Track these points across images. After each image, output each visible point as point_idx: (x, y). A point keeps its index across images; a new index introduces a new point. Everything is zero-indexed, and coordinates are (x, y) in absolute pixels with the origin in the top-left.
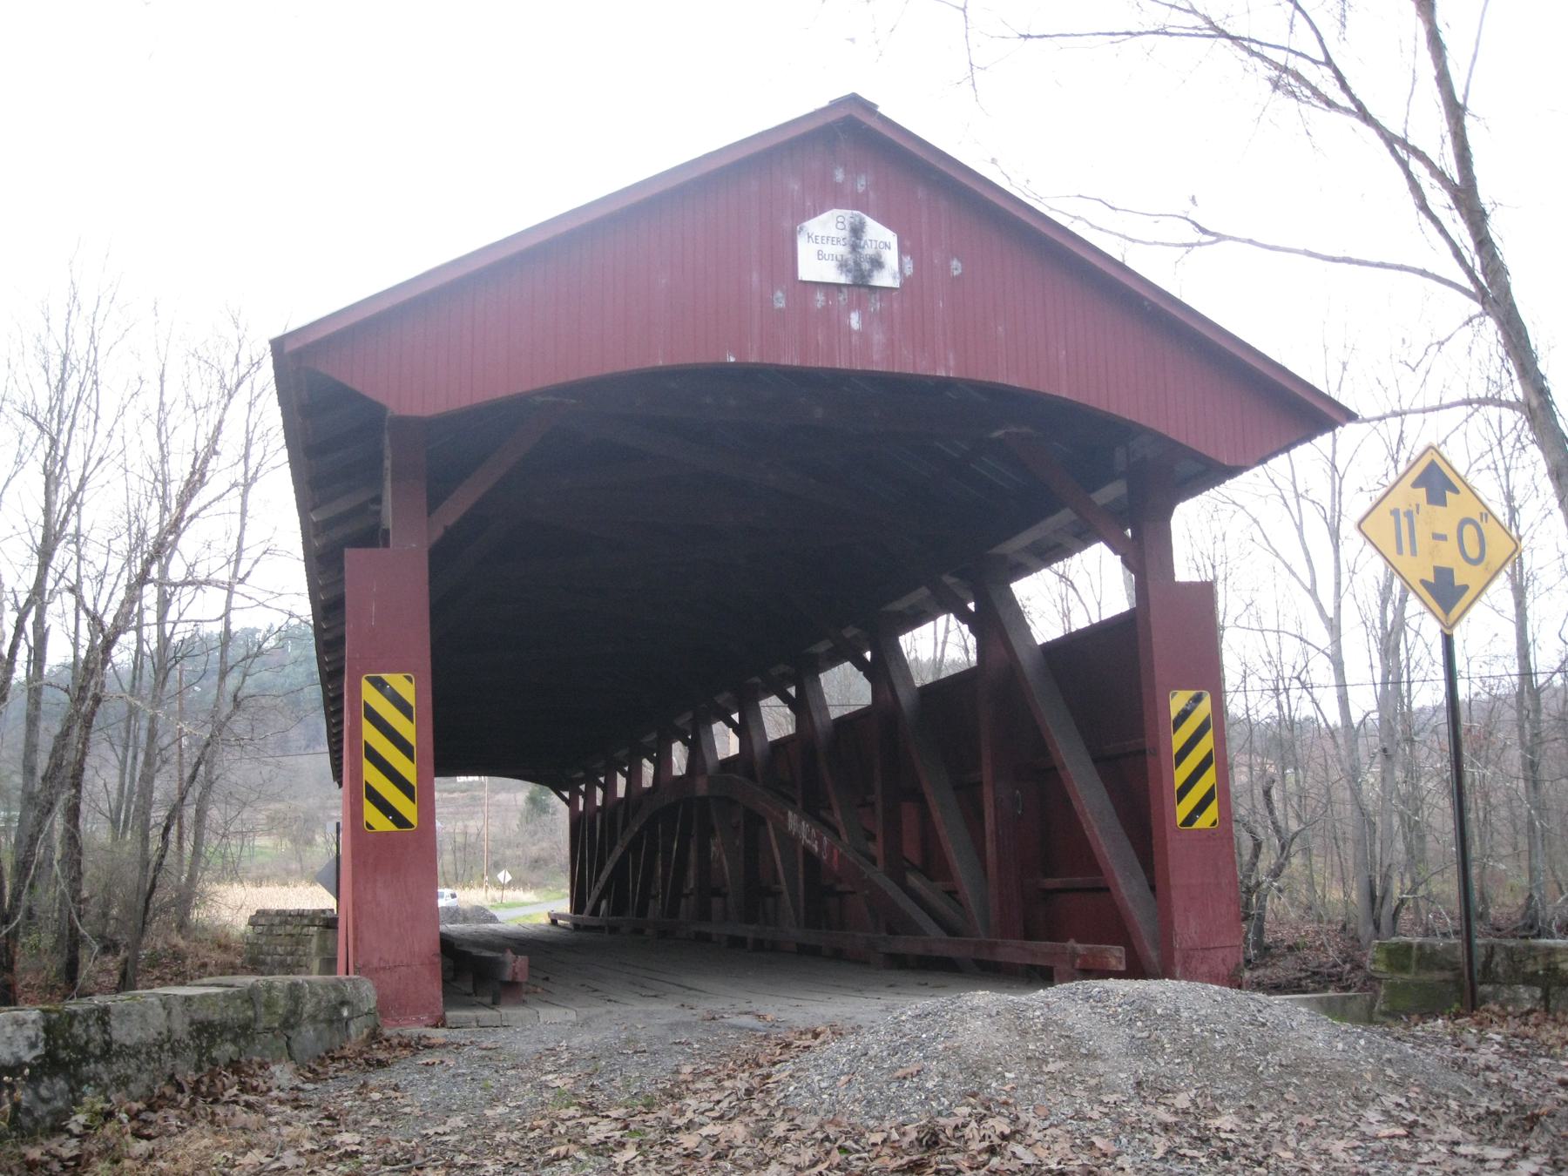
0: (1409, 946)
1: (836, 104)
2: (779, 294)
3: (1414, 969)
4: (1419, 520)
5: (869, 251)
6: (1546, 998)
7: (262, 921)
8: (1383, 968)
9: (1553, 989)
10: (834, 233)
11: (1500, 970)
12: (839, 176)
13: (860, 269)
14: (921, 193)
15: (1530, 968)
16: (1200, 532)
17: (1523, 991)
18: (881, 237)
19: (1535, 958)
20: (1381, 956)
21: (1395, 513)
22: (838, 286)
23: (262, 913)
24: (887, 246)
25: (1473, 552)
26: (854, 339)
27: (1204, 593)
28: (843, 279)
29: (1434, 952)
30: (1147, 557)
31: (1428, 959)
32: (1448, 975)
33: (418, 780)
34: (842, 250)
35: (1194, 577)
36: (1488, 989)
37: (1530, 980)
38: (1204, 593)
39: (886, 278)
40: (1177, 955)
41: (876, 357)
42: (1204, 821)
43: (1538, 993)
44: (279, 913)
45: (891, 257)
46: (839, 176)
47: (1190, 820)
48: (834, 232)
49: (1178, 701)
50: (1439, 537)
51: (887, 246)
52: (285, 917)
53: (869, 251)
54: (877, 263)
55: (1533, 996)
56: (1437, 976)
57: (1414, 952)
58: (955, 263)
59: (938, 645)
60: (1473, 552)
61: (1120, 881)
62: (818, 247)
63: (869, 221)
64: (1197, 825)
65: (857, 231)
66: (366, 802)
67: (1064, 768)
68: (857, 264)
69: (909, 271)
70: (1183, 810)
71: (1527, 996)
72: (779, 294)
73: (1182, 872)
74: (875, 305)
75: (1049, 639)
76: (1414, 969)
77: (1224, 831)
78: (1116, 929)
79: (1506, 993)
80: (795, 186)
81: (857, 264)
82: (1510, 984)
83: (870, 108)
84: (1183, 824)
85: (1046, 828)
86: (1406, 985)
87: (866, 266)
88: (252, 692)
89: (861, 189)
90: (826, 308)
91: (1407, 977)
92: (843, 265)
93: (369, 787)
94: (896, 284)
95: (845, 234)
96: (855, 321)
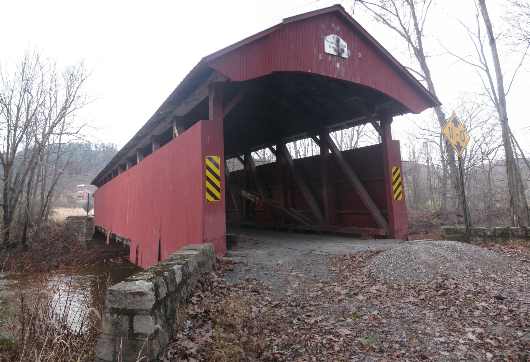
0: (451, 229)
1: (335, 6)
2: (320, 55)
4: (453, 130)
5: (341, 47)
6: (484, 240)
7: (70, 219)
10: (333, 41)
12: (333, 26)
13: (340, 52)
14: (351, 34)
15: (479, 234)
16: (402, 126)
18: (343, 43)
20: (444, 231)
21: (449, 128)
22: (334, 55)
23: (69, 217)
24: (345, 47)
25: (463, 139)
26: (338, 70)
27: (397, 142)
28: (335, 54)
29: (457, 230)
30: (384, 130)
32: (461, 235)
34: (335, 46)
35: (396, 139)
36: (471, 238)
37: (480, 236)
38: (397, 142)
39: (345, 55)
41: (343, 76)
42: (400, 199)
43: (482, 239)
44: (74, 217)
45: (346, 49)
46: (333, 26)
48: (333, 41)
50: (457, 135)
51: (345, 47)
52: (76, 218)
53: (341, 47)
54: (343, 51)
58: (359, 54)
59: (303, 148)
60: (463, 139)
62: (329, 44)
63: (341, 39)
65: (338, 41)
66: (207, 181)
67: (354, 184)
68: (338, 50)
69: (350, 54)
70: (395, 196)
71: (480, 240)
72: (320, 55)
73: (396, 211)
74: (343, 62)
77: (403, 201)
78: (375, 224)
79: (475, 239)
80: (323, 26)
81: (338, 50)
83: (343, 9)
85: (357, 199)
87: (340, 51)
88: (495, 164)
89: (338, 30)
90: (331, 61)
92: (335, 50)
93: (207, 177)
94: (347, 57)
95: (335, 41)
96: (338, 65)
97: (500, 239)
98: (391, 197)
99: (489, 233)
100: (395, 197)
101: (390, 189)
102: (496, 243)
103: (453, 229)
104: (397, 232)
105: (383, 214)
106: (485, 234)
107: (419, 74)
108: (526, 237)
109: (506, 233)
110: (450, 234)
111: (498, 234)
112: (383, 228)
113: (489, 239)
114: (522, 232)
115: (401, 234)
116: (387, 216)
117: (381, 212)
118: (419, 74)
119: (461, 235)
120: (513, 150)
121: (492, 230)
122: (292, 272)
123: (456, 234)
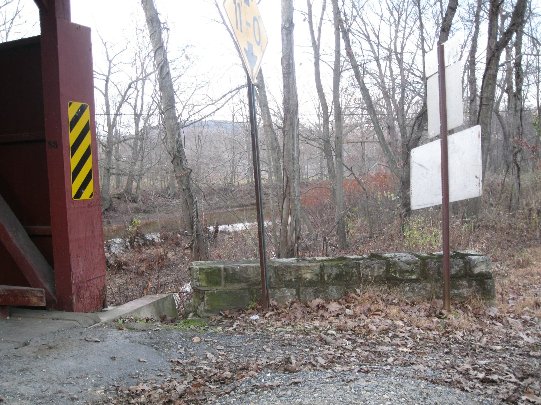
0: (219, 270)
3: (223, 283)
6: (298, 294)
8: (204, 284)
9: (301, 289)
11: (272, 280)
15: (287, 278)
17: (287, 292)
19: (290, 272)
20: (202, 276)
29: (235, 273)
31: (231, 276)
32: (243, 285)
33: (84, 200)
37: (289, 285)
40: (74, 288)
42: (86, 195)
43: (294, 291)
47: (79, 194)
49: (72, 111)
55: (292, 294)
56: (236, 287)
57: (223, 273)
61: (11, 234)
64: (83, 197)
73: (77, 230)
75: (27, 36)
76: (223, 283)
78: (16, 273)
82: (279, 288)
84: (75, 197)
86: (220, 293)
91: (220, 288)
97: (333, 291)
98: (63, 190)
99: (308, 276)
100: (74, 193)
101: (61, 163)
102: (328, 301)
103: (226, 270)
104: (79, 288)
105: (34, 237)
106: (299, 278)
107: (142, 104)
108: (388, 279)
109: (347, 274)
110: (217, 283)
111: (329, 277)
112: (37, 284)
113: (310, 290)
114: (380, 268)
115: (88, 293)
116: (51, 245)
117: (28, 230)
118: (142, 104)
119: (243, 285)
120: (333, 111)
121: (317, 269)
122: (290, 340)
123: (232, 282)
